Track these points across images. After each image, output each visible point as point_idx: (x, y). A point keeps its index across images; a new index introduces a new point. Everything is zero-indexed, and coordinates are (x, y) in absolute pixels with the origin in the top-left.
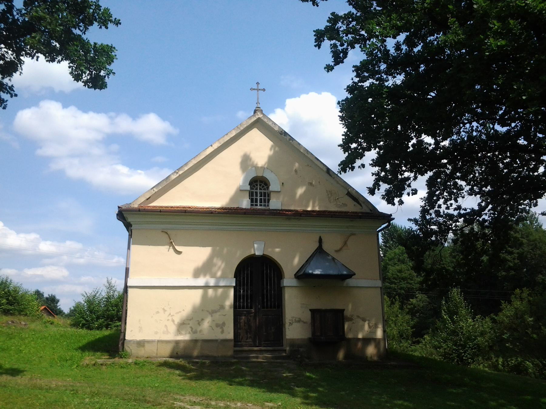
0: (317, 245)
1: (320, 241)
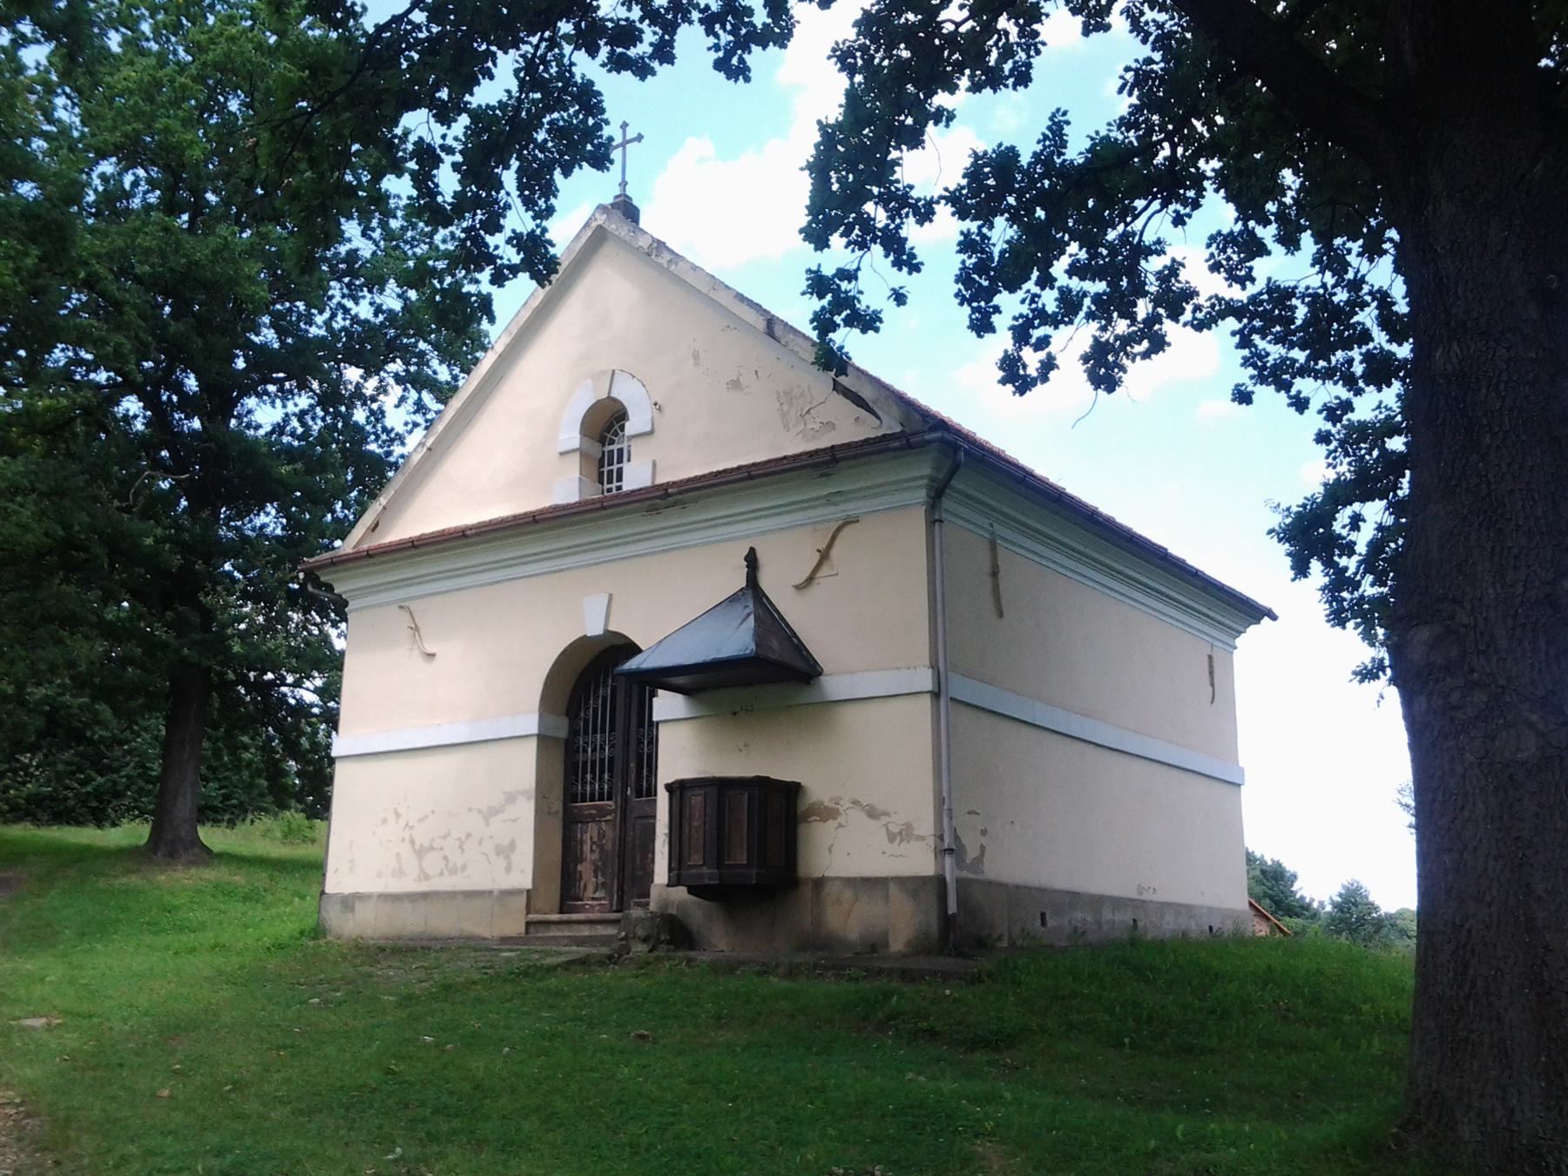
1: (752, 560)
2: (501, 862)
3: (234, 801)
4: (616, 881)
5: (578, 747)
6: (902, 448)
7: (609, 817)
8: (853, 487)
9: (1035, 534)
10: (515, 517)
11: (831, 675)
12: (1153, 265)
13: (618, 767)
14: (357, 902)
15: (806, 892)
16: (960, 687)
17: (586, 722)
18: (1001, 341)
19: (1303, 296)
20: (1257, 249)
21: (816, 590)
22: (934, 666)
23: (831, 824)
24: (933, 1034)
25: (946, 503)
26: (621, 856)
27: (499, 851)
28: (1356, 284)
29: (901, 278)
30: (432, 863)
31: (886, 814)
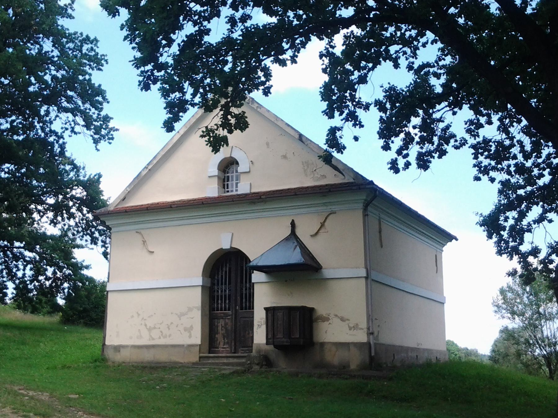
0: (289, 232)
1: (293, 224)
4: (233, 341)
5: (215, 290)
7: (229, 317)
10: (189, 201)
11: (326, 269)
12: (441, 125)
14: (121, 348)
16: (374, 275)
19: (494, 142)
20: (480, 126)
21: (319, 237)
22: (366, 268)
23: (326, 323)
25: (369, 208)
26: (235, 332)
27: (185, 329)
28: (512, 138)
29: (357, 131)
31: (348, 320)
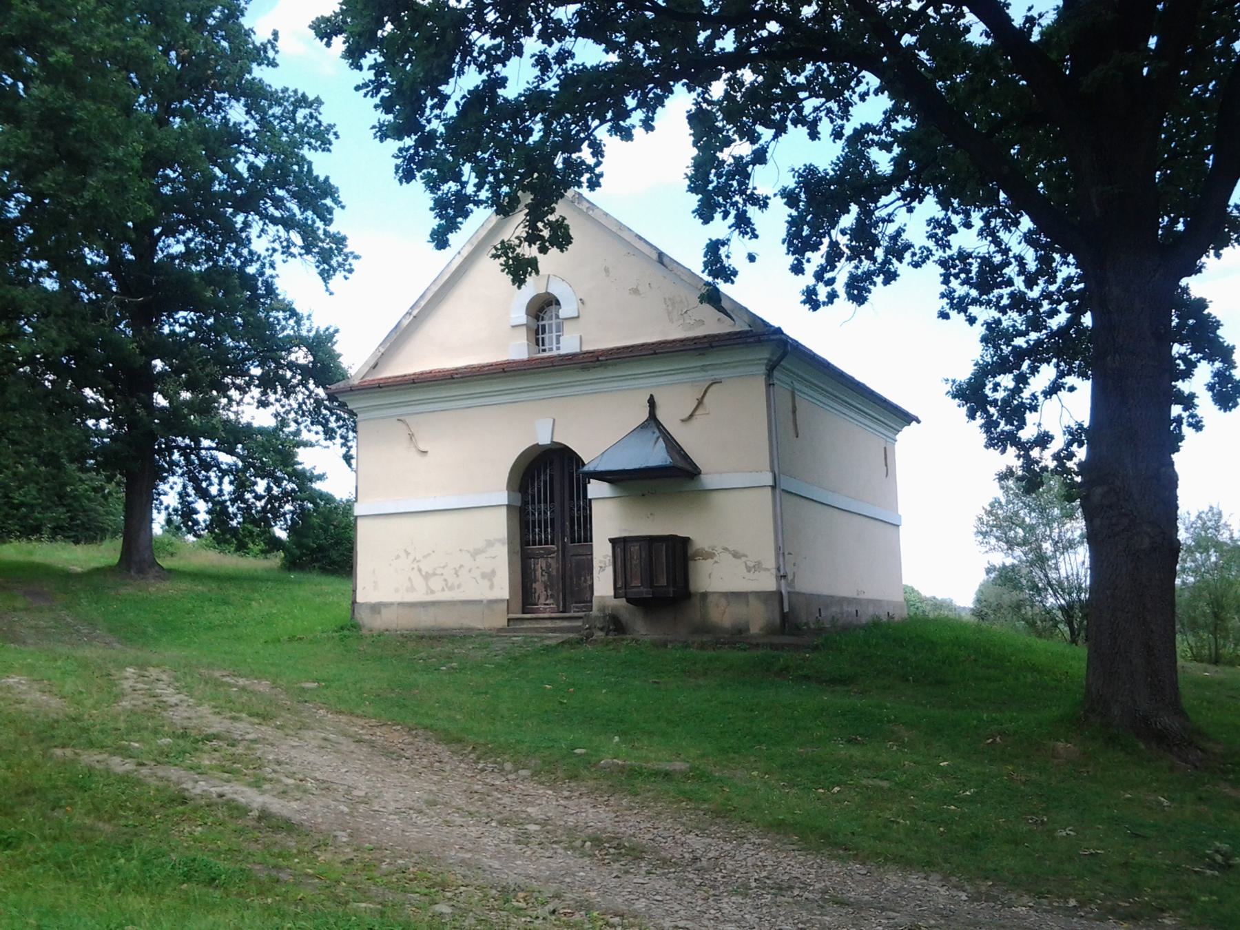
0: (645, 415)
1: (652, 403)
2: (486, 583)
3: (78, 522)
6: (755, 342)
8: (719, 362)
9: (811, 385)
10: (482, 367)
13: (558, 525)
15: (696, 601)
16: (785, 483)
17: (533, 496)
18: (808, 279)
20: (951, 230)
22: (773, 471)
23: (710, 561)
24: (807, 678)
25: (776, 373)
26: (564, 578)
27: (484, 576)
28: (1005, 252)
30: (436, 584)
